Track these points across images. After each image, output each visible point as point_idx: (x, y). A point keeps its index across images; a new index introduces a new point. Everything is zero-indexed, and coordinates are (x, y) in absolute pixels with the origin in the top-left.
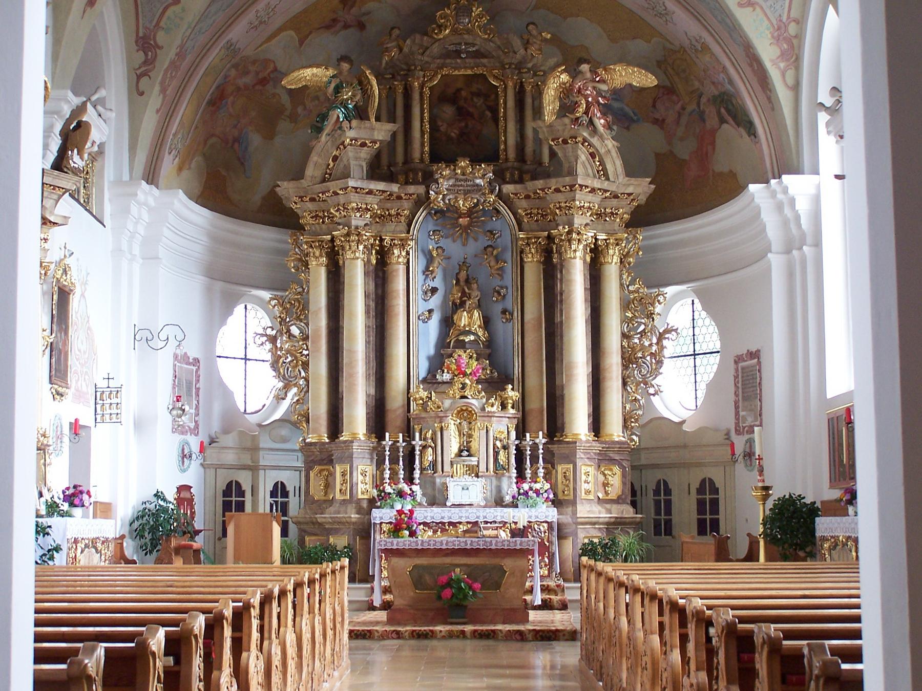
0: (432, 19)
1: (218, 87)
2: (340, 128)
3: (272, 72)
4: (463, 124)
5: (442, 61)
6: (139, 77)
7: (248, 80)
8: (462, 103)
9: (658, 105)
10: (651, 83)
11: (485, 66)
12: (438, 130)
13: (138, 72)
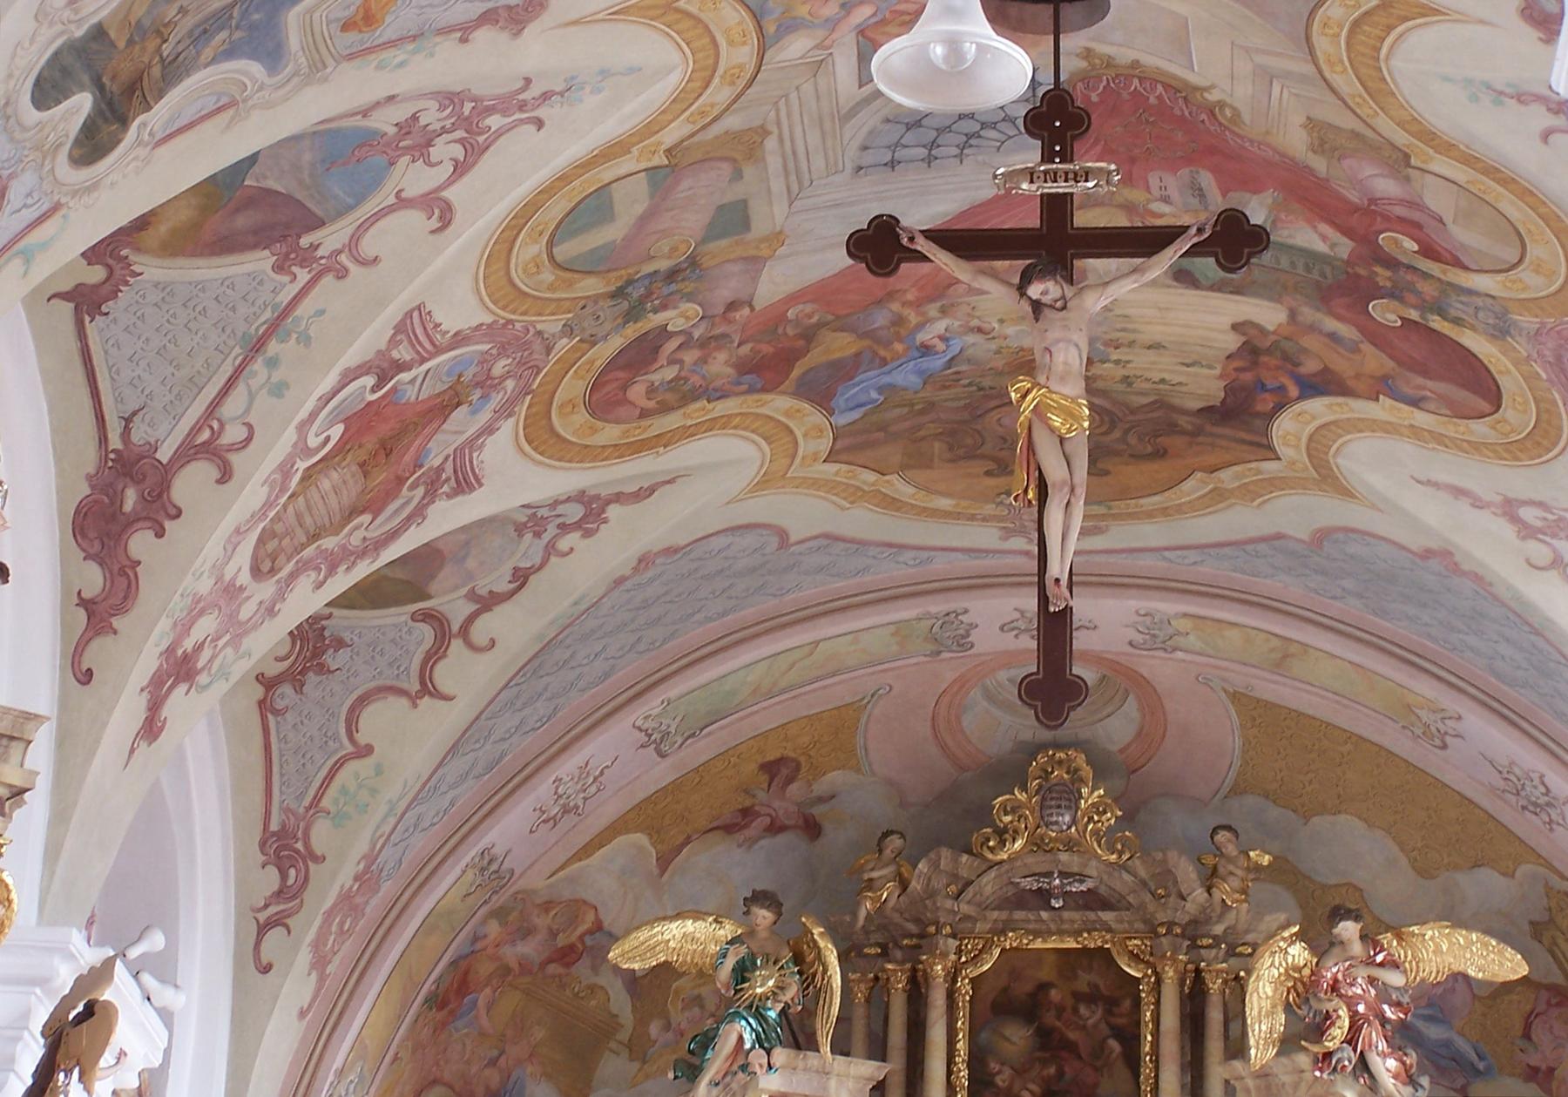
0: (983, 815)
1: (454, 963)
2: (744, 1068)
3: (590, 932)
4: (1052, 1070)
5: (1004, 915)
6: (263, 929)
7: (529, 949)
8: (1050, 1019)
9: (1538, 1032)
10: (1514, 971)
11: (1109, 930)
12: (991, 1084)
13: (262, 917)
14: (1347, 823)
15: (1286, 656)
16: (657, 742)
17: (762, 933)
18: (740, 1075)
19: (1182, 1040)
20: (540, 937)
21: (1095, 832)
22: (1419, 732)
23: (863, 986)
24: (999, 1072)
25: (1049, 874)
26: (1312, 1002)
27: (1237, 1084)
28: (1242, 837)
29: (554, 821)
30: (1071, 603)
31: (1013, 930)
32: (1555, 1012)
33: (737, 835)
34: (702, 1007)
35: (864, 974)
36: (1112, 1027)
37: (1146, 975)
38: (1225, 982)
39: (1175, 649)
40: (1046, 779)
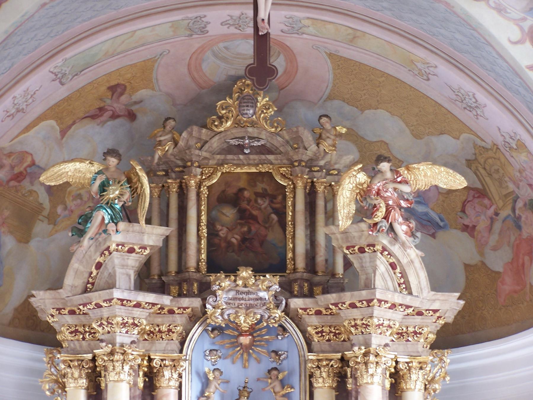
0: (211, 109)
2: (105, 231)
3: (30, 166)
5: (222, 157)
8: (244, 205)
9: (469, 210)
11: (271, 164)
12: (217, 235)
14: (382, 113)
15: (354, 37)
16: (60, 78)
17: (112, 169)
18: (103, 235)
19: (306, 214)
20: (7, 169)
21: (265, 118)
22: (416, 73)
23: (157, 190)
24: (221, 230)
25: (243, 138)
26: (368, 200)
27: (332, 236)
28: (333, 120)
29: (13, 115)
30: (270, 31)
31: (227, 164)
32: (477, 201)
33: (96, 120)
34: (81, 199)
35: (157, 184)
36: (273, 208)
37: (289, 185)
38: (325, 187)
39: (303, 33)
40: (241, 93)
